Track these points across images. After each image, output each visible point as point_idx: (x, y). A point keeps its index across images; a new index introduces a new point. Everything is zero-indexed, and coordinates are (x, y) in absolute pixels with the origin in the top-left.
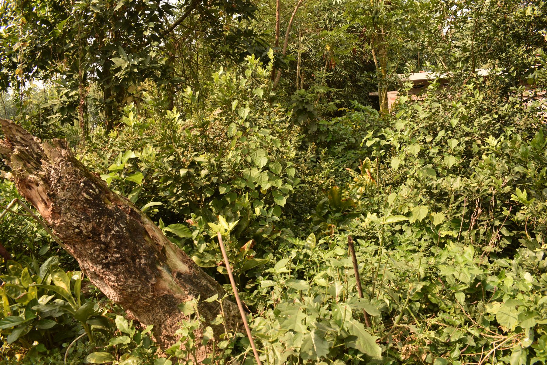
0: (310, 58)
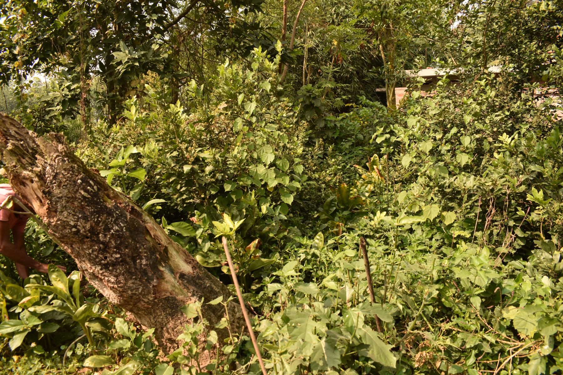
0: (316, 53)
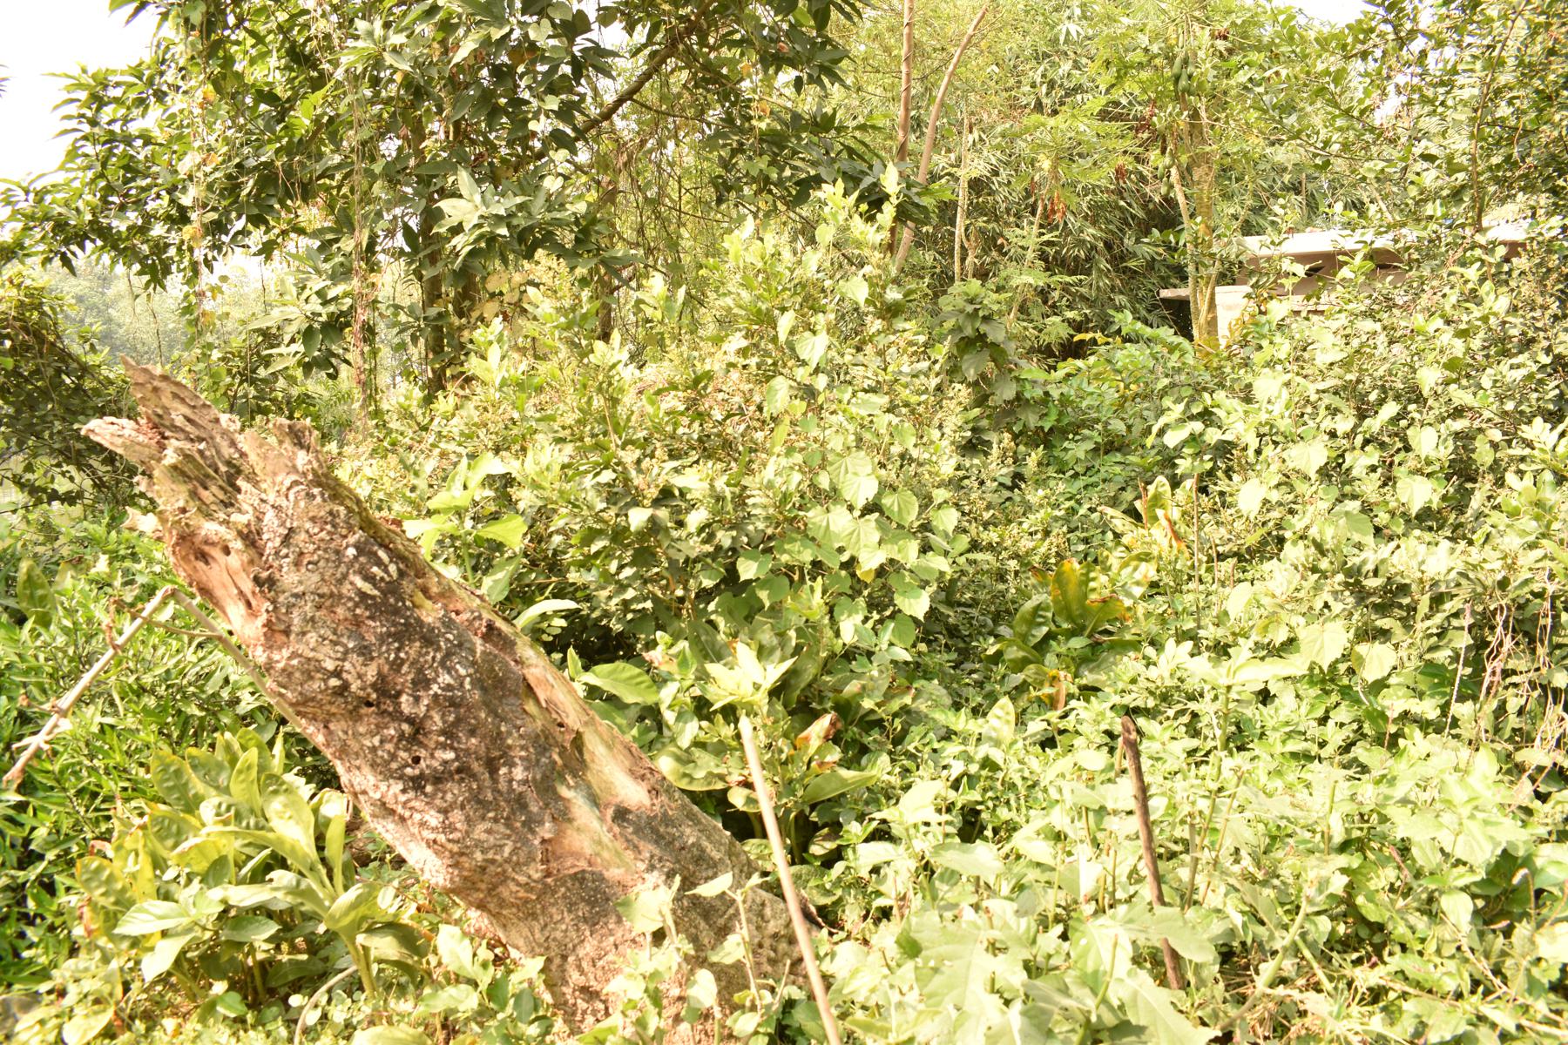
0: (992, 193)
